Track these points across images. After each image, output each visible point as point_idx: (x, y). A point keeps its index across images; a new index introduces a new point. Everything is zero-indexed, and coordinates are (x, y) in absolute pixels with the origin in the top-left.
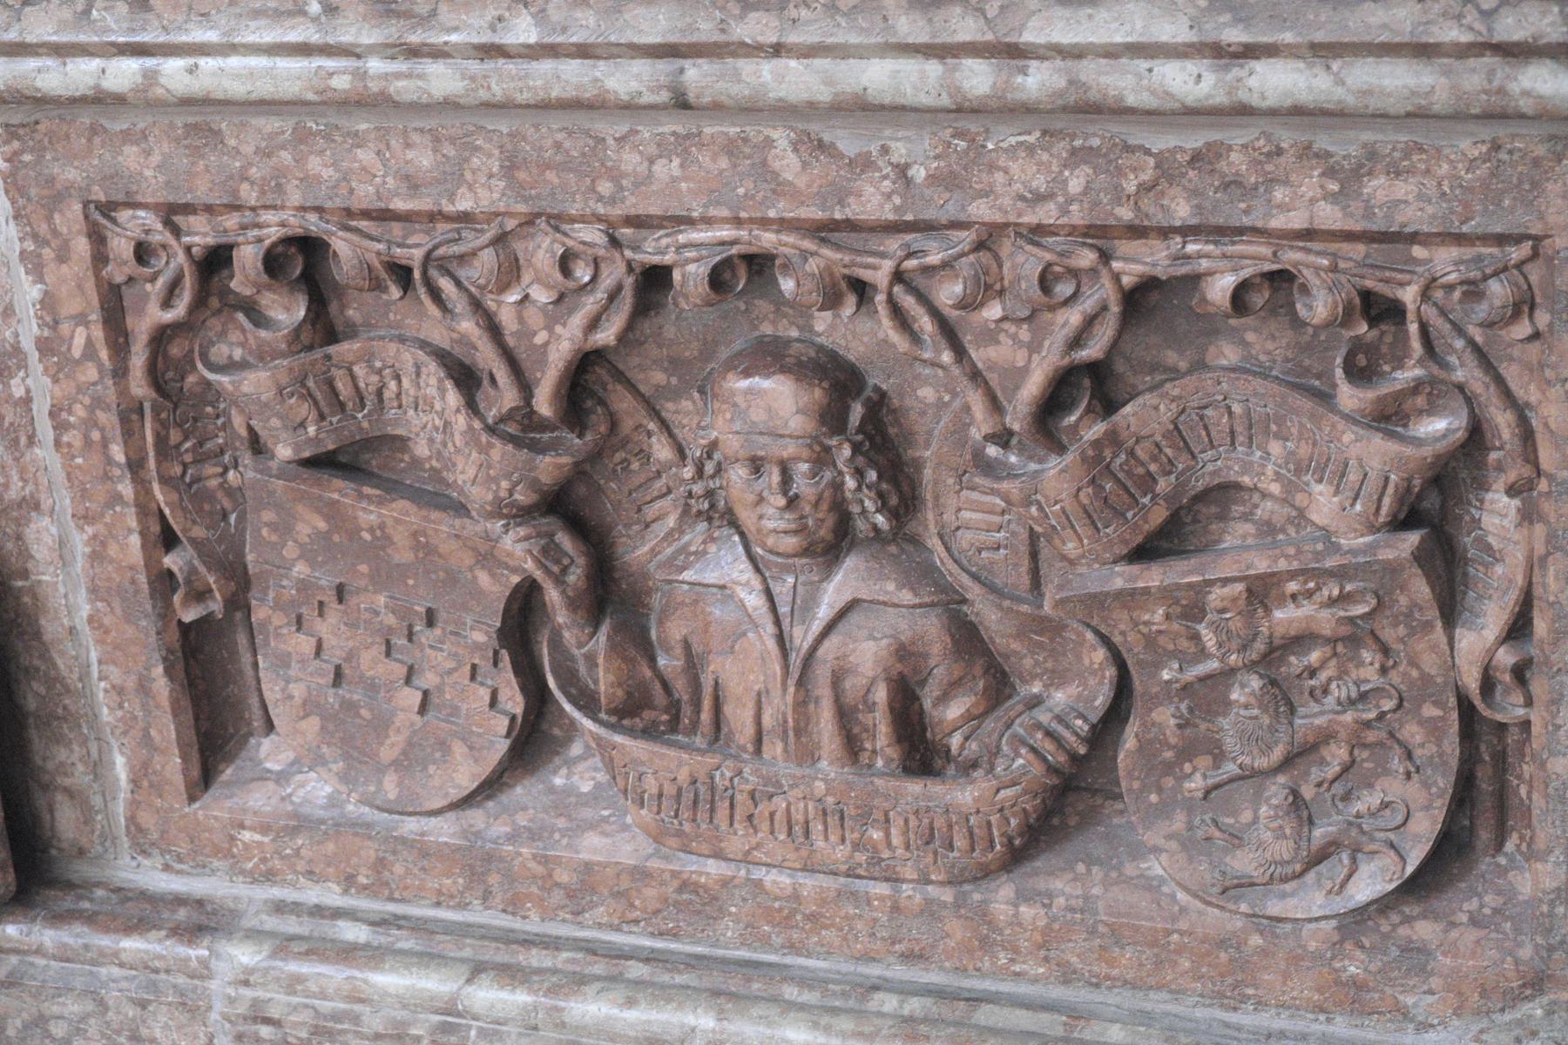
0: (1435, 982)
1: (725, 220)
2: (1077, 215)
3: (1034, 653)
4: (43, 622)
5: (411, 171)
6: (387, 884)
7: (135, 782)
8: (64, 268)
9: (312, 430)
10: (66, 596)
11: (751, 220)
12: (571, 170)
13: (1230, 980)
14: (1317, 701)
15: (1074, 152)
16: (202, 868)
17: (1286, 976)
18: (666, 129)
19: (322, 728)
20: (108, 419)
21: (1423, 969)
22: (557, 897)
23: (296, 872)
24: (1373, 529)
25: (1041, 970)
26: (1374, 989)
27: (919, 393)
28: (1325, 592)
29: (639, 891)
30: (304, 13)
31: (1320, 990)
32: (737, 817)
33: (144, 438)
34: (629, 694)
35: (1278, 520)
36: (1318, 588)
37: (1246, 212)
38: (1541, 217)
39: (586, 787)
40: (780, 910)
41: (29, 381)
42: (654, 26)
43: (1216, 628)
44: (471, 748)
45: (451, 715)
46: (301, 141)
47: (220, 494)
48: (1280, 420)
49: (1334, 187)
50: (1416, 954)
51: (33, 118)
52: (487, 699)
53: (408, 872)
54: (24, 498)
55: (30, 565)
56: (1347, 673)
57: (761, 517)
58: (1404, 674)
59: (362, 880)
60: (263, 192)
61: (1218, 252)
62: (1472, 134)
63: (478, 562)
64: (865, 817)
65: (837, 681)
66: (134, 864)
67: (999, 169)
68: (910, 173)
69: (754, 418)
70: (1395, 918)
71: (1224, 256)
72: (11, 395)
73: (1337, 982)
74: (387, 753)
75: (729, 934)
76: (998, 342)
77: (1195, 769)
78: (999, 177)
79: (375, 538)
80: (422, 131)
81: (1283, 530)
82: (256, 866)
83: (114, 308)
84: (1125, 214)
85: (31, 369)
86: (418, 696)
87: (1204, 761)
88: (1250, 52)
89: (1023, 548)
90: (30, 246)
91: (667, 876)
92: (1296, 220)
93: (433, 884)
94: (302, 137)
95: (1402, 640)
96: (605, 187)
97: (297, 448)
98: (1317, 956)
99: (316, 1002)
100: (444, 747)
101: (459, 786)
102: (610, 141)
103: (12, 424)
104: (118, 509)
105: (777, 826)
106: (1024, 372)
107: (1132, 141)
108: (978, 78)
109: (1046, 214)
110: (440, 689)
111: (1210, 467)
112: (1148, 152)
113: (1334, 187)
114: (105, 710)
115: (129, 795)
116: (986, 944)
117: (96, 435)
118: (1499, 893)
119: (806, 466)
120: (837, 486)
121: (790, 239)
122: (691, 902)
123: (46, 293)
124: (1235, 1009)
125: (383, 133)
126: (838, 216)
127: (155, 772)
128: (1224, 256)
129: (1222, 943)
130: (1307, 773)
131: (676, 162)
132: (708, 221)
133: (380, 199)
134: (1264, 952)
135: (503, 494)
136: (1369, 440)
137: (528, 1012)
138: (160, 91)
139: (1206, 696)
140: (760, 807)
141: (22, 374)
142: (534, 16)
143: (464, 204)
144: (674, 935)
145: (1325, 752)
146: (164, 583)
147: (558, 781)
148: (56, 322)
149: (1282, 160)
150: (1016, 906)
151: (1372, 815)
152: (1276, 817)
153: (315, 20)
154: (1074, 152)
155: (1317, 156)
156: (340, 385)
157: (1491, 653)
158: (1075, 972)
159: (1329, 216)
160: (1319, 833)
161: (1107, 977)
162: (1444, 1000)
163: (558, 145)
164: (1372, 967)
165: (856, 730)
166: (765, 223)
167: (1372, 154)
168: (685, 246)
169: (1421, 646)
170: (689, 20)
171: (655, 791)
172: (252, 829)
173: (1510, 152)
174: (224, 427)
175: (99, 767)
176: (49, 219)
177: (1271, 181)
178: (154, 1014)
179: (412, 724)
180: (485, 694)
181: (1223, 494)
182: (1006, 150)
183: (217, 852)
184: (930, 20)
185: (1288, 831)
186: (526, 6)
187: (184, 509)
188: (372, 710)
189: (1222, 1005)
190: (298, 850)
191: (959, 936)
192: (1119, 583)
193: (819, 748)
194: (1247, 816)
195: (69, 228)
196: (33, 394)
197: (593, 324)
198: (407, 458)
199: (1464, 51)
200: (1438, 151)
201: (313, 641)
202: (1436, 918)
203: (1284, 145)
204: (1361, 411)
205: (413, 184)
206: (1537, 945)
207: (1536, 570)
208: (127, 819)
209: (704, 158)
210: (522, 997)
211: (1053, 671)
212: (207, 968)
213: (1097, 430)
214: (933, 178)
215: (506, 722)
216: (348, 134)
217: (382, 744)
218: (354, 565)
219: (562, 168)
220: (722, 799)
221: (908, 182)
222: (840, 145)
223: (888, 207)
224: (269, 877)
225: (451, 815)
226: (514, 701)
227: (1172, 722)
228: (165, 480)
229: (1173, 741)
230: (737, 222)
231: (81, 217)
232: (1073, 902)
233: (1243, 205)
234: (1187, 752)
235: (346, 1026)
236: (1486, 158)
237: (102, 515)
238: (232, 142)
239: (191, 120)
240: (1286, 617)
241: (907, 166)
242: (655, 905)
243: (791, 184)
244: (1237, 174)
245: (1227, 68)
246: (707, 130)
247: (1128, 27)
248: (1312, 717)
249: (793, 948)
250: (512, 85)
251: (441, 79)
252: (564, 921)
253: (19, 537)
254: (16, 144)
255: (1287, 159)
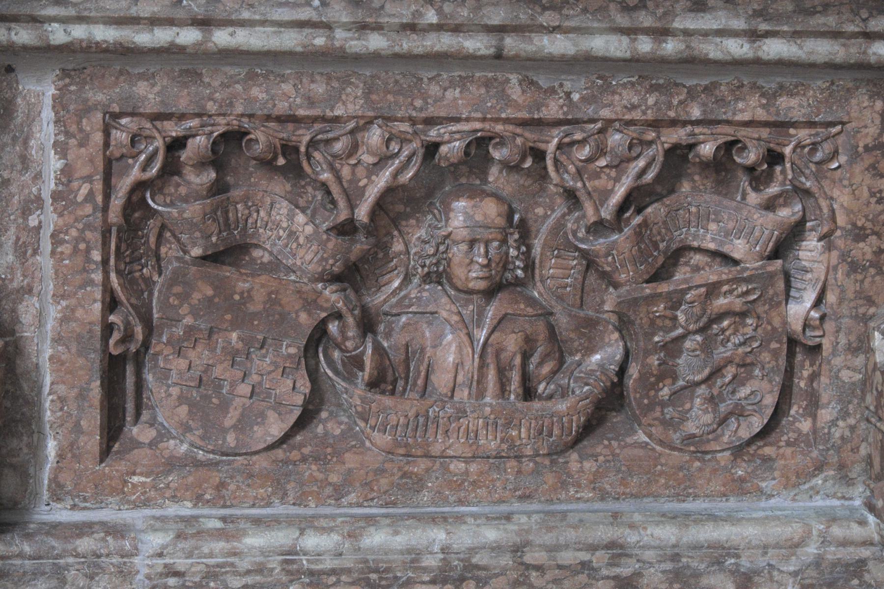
0: (777, 474)
1: (478, 120)
2: (650, 115)
3: (579, 338)
4: (18, 362)
5: (312, 95)
6: (224, 497)
7: (61, 456)
8: (83, 150)
9: (214, 239)
10: (37, 344)
11: (492, 120)
12: (402, 94)
13: (682, 487)
14: (724, 346)
15: (651, 86)
16: (101, 505)
17: (709, 480)
18: (456, 74)
19: (189, 411)
20: (93, 237)
21: (771, 468)
22: (329, 490)
23: (164, 498)
24: (762, 259)
25: (591, 495)
26: (749, 481)
27: (536, 211)
28: (740, 290)
29: (377, 481)
30: (311, 6)
31: (724, 486)
32: (440, 431)
33: (110, 247)
34: (379, 373)
35: (701, 265)
36: (737, 288)
37: (725, 113)
38: (848, 114)
39: (338, 432)
40: (457, 480)
41: (42, 217)
42: (497, 16)
43: (685, 313)
44: (280, 414)
45: (266, 397)
46: (251, 79)
47: (140, 281)
48: (716, 213)
49: (764, 101)
50: (767, 460)
51: (82, 66)
52: (291, 385)
53: (238, 488)
54: (22, 287)
55: (17, 328)
56: (738, 331)
57: (469, 271)
58: (765, 328)
59: (207, 497)
60: (221, 106)
61: (710, 132)
62: (822, 78)
63: (304, 306)
64: (508, 425)
65: (497, 354)
66: (48, 508)
67: (617, 93)
68: (572, 96)
69: (477, 219)
70: (754, 447)
71: (712, 134)
72: (27, 225)
73: (733, 480)
74: (228, 422)
75: (425, 499)
76: (600, 178)
77: (664, 386)
78: (617, 97)
79: (242, 297)
80: (322, 74)
81: (703, 269)
82: (139, 497)
83: (109, 170)
84: (672, 114)
85: (45, 209)
86: (249, 389)
87: (668, 381)
88: (768, 34)
89: (579, 286)
90: (62, 138)
91: (395, 470)
92: (746, 117)
93: (252, 493)
94: (252, 77)
95: (766, 312)
96: (418, 103)
97: (205, 249)
98: (725, 468)
99: (204, 560)
100: (262, 415)
101: (273, 436)
102: (425, 80)
103: (24, 242)
104: (88, 289)
105: (461, 435)
106: (611, 192)
107: (678, 81)
108: (645, 45)
109: (636, 115)
110: (260, 383)
111: (678, 238)
112: (684, 86)
113: (764, 101)
114: (48, 413)
115: (55, 465)
116: (564, 485)
117: (82, 246)
118: (794, 432)
119: (497, 243)
120: (507, 254)
121: (511, 128)
122: (406, 483)
123: (66, 165)
124: (684, 501)
125: (299, 76)
126: (536, 116)
127: (78, 448)
128: (712, 134)
129: (681, 468)
130: (716, 382)
131: (458, 90)
132: (468, 120)
133: (291, 110)
134: (700, 470)
135: (328, 267)
136: (767, 216)
137: (339, 545)
138: (210, 45)
139: (673, 348)
140: (453, 425)
141: (39, 212)
142: (436, 10)
143: (338, 112)
144: (394, 504)
145: (724, 371)
146: (108, 329)
147: (320, 429)
148: (70, 181)
149: (744, 89)
150: (581, 463)
151: (746, 398)
152: (705, 403)
153: (316, 9)
154: (651, 86)
155: (758, 88)
156: (231, 215)
157: (809, 312)
158: (607, 493)
159: (761, 115)
160: (723, 408)
161: (624, 494)
162: (779, 481)
163: (396, 82)
164: (749, 470)
165: (504, 380)
166: (497, 120)
167: (781, 87)
168: (455, 133)
169: (774, 314)
170: (515, 14)
171: (395, 423)
172: (141, 474)
173: (838, 86)
174: (144, 244)
175: (36, 449)
176: (79, 123)
177: (737, 100)
178: (98, 582)
179: (244, 405)
180: (289, 383)
181: (684, 249)
182: (622, 85)
183: (114, 491)
184: (631, 17)
185: (710, 410)
186: (432, 5)
187: (126, 288)
188: (219, 398)
189: (678, 500)
190: (168, 484)
191: (550, 482)
192: (648, 291)
193: (486, 391)
194: (687, 406)
195: (92, 128)
196: (43, 224)
197: (395, 175)
198: (247, 258)
199: (854, 35)
200: (809, 85)
201: (187, 362)
202: (771, 444)
203: (745, 83)
204: (760, 205)
205: (311, 102)
206: (819, 450)
207: (831, 272)
208: (50, 480)
209: (473, 88)
210: (335, 537)
211: (588, 348)
212: (137, 549)
213: (638, 220)
214: (583, 99)
215: (303, 397)
216: (279, 75)
217: (225, 417)
218: (223, 315)
219: (399, 92)
220: (433, 423)
221: (571, 100)
222: (541, 83)
223: (560, 112)
224: (146, 503)
225: (264, 455)
226: (304, 385)
227: (656, 363)
228: (119, 272)
229: (655, 372)
230: (484, 120)
231: (101, 122)
232: (607, 458)
233: (723, 110)
234: (661, 378)
235: (228, 569)
236: (828, 88)
237: (75, 294)
238: (207, 80)
239: (184, 67)
240: (721, 302)
241: (570, 93)
242: (386, 488)
243: (516, 101)
244: (723, 96)
245: (754, 42)
246: (477, 75)
247: (719, 22)
248: (722, 353)
249: (460, 502)
250: (414, 44)
251: (376, 42)
252: (329, 505)
253: (14, 311)
254: (67, 80)
255: (745, 89)
